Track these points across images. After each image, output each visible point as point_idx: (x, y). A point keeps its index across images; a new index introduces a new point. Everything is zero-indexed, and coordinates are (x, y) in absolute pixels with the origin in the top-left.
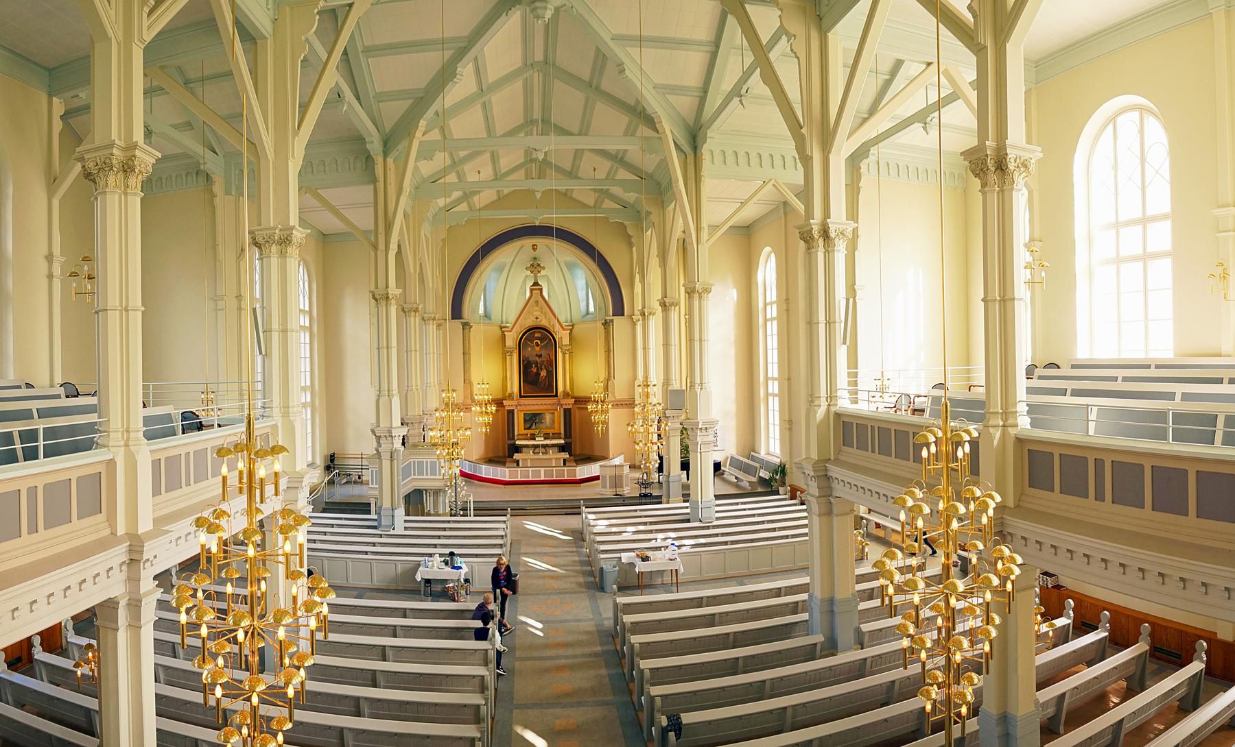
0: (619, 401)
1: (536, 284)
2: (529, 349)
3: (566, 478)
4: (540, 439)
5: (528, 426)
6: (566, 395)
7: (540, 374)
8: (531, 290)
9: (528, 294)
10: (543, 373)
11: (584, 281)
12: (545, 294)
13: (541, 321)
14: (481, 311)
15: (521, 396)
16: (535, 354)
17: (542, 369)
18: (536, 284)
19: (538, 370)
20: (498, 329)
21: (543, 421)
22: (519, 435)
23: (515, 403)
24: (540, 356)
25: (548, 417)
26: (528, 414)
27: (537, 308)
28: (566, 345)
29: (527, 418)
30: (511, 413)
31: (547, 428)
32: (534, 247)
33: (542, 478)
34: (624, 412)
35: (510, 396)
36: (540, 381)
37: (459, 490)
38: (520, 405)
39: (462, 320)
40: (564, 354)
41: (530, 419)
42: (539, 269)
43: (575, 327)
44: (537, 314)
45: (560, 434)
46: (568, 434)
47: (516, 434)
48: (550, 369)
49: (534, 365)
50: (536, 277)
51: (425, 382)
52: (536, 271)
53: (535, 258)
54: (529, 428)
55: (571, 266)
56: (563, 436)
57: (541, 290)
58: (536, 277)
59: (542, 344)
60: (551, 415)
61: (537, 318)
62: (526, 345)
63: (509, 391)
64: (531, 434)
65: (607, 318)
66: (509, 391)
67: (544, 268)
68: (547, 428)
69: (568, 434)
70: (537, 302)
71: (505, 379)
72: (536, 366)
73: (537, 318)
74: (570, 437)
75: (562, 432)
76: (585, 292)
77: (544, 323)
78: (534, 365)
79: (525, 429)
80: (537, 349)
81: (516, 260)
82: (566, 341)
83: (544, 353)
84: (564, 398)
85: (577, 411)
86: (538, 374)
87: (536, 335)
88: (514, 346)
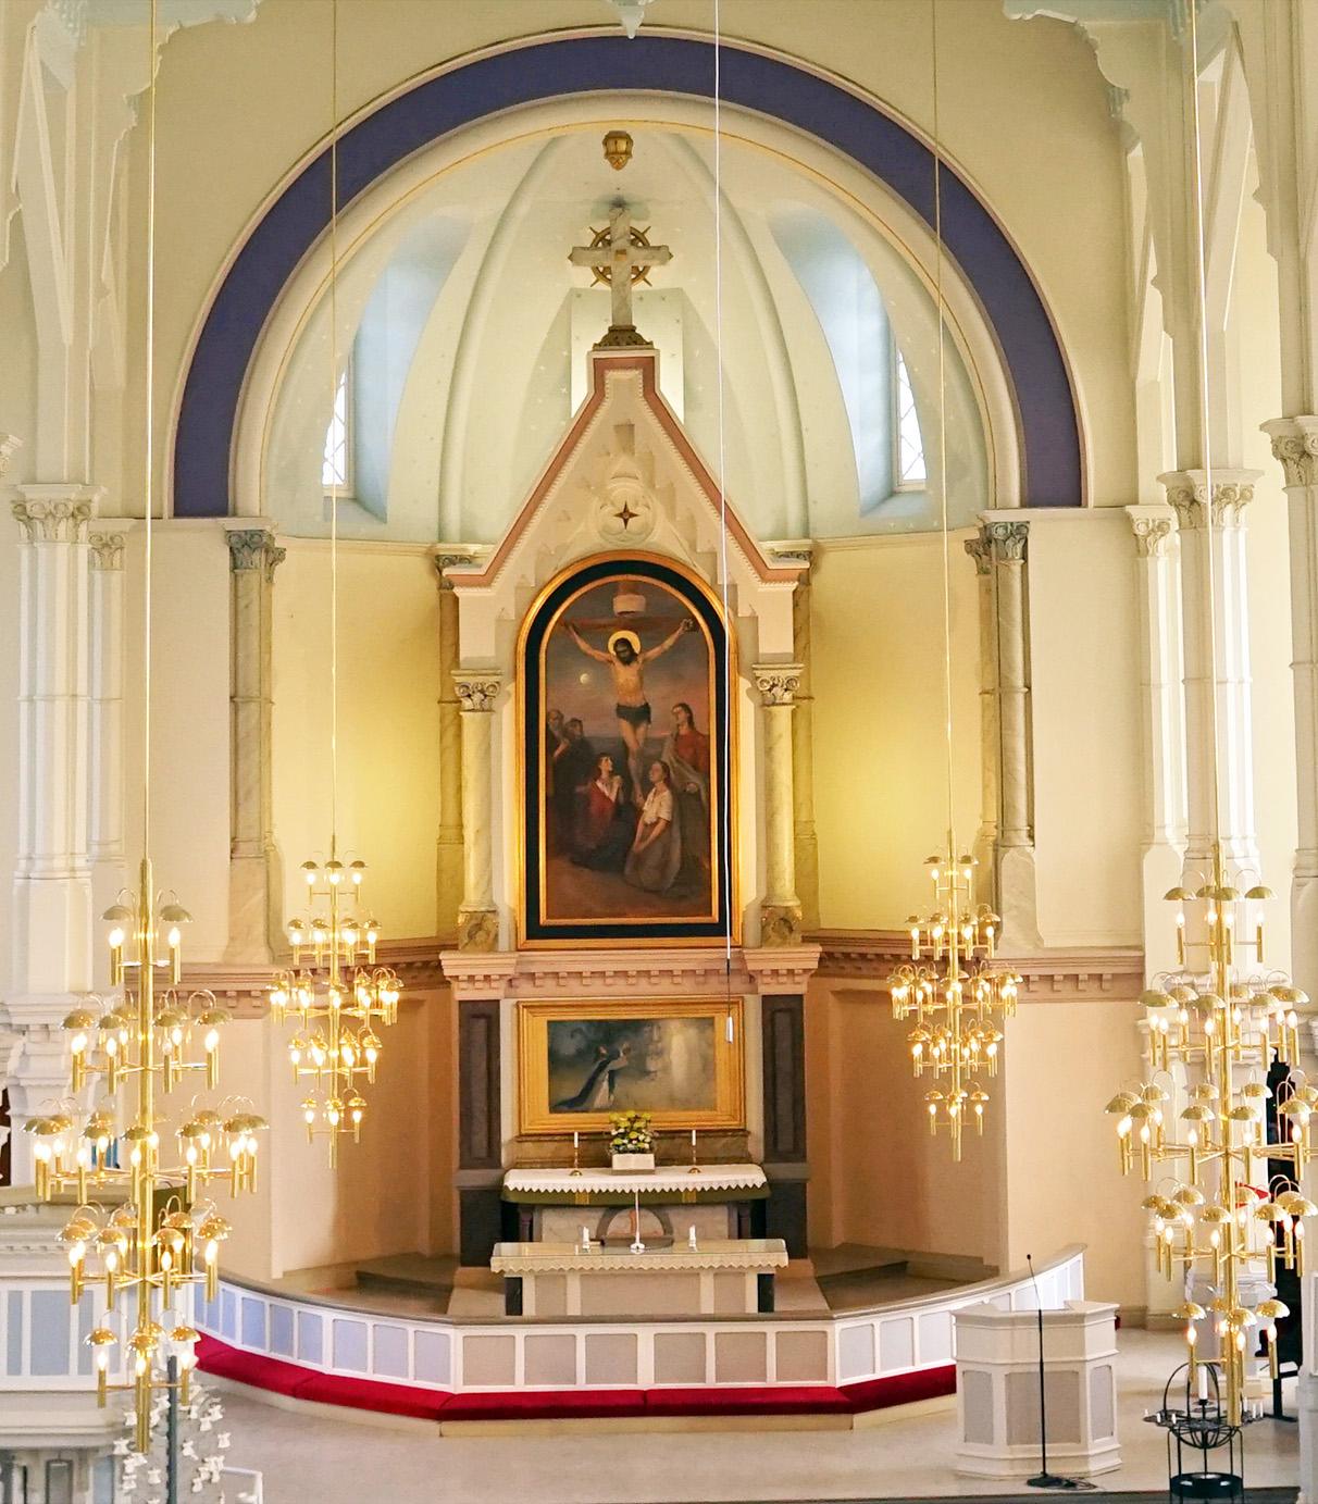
0: (1052, 962)
1: (622, 334)
2: (584, 678)
3: (772, 1381)
4: (634, 1162)
5: (571, 1090)
6: (777, 923)
7: (639, 812)
8: (599, 369)
9: (581, 390)
10: (657, 807)
11: (874, 325)
12: (670, 387)
13: (647, 530)
14: (334, 473)
15: (535, 931)
16: (612, 701)
17: (648, 787)
18: (622, 334)
19: (627, 787)
20: (419, 568)
21: (652, 1065)
22: (521, 1138)
23: (502, 963)
24: (640, 715)
25: (678, 1043)
26: (574, 1028)
27: (623, 463)
28: (776, 660)
29: (569, 1047)
30: (482, 1017)
31: (673, 1102)
32: (617, 146)
33: (646, 1379)
34: (1088, 1016)
35: (480, 930)
36: (638, 846)
37: (188, 1450)
38: (532, 976)
39: (229, 523)
40: (766, 705)
41: (580, 1053)
42: (637, 257)
43: (829, 563)
44: (625, 491)
45: (744, 1133)
46: (786, 1142)
47: (507, 1131)
48: (694, 783)
49: (606, 765)
50: (622, 303)
51: (23, 850)
52: (621, 270)
53: (619, 204)
54: (578, 1103)
55: (800, 245)
56: (756, 1146)
57: (649, 368)
58: (622, 303)
59: (654, 653)
60: (692, 1032)
61: (626, 515)
62: (566, 654)
63: (473, 899)
64: (590, 1137)
65: (995, 516)
66: (473, 899)
67: (664, 254)
68: (673, 1102)
69: (786, 1142)
70: (627, 430)
71: (452, 834)
72: (620, 768)
73: (626, 515)
74: (797, 1153)
75: (755, 1122)
76: (875, 381)
77: (662, 537)
78: (606, 765)
79: (556, 1107)
80: (626, 675)
81: (523, 209)
82: (776, 638)
83: (661, 698)
84: (764, 940)
85: (833, 1006)
86: (627, 811)
87: (624, 603)
88: (506, 668)
